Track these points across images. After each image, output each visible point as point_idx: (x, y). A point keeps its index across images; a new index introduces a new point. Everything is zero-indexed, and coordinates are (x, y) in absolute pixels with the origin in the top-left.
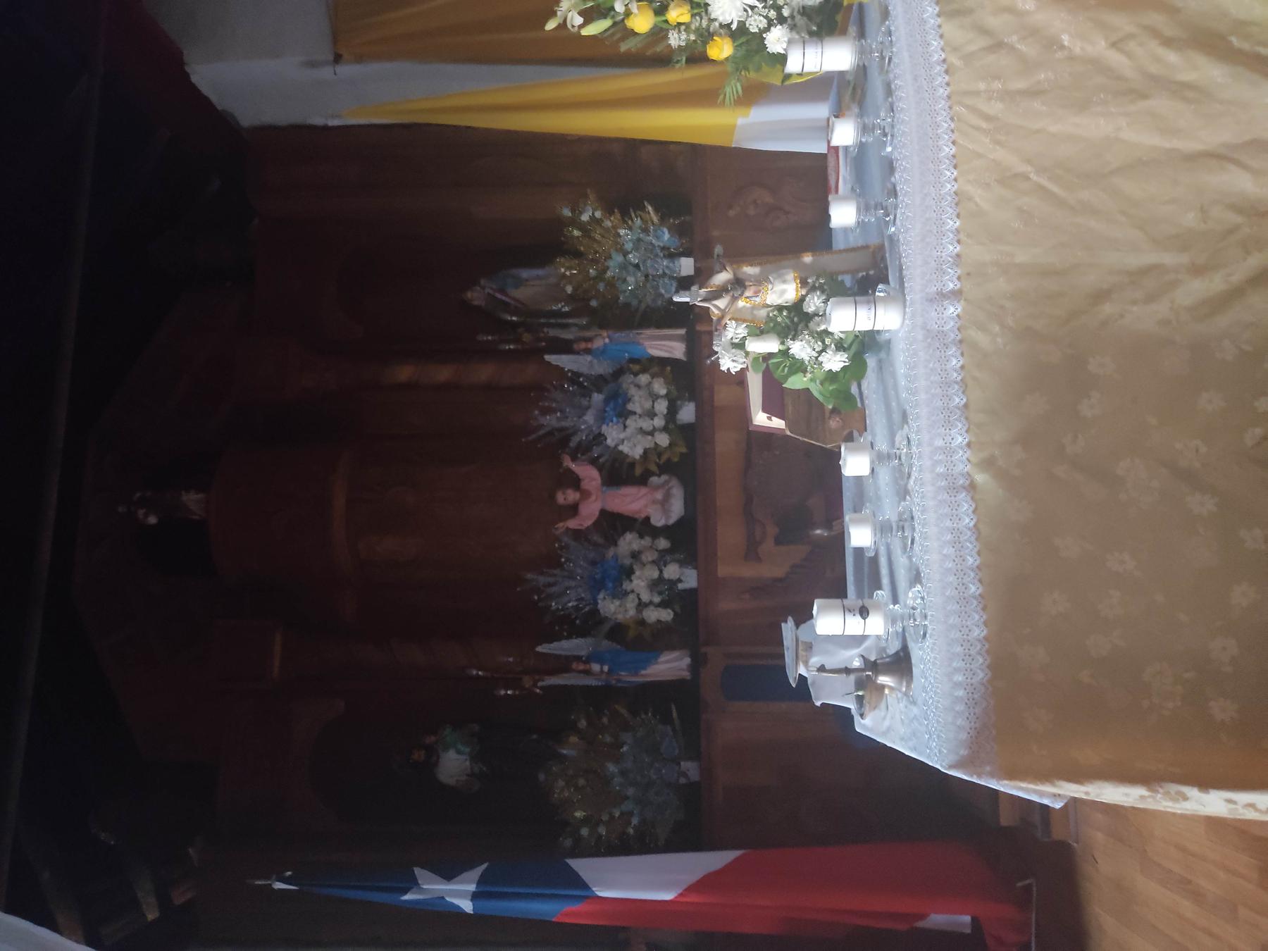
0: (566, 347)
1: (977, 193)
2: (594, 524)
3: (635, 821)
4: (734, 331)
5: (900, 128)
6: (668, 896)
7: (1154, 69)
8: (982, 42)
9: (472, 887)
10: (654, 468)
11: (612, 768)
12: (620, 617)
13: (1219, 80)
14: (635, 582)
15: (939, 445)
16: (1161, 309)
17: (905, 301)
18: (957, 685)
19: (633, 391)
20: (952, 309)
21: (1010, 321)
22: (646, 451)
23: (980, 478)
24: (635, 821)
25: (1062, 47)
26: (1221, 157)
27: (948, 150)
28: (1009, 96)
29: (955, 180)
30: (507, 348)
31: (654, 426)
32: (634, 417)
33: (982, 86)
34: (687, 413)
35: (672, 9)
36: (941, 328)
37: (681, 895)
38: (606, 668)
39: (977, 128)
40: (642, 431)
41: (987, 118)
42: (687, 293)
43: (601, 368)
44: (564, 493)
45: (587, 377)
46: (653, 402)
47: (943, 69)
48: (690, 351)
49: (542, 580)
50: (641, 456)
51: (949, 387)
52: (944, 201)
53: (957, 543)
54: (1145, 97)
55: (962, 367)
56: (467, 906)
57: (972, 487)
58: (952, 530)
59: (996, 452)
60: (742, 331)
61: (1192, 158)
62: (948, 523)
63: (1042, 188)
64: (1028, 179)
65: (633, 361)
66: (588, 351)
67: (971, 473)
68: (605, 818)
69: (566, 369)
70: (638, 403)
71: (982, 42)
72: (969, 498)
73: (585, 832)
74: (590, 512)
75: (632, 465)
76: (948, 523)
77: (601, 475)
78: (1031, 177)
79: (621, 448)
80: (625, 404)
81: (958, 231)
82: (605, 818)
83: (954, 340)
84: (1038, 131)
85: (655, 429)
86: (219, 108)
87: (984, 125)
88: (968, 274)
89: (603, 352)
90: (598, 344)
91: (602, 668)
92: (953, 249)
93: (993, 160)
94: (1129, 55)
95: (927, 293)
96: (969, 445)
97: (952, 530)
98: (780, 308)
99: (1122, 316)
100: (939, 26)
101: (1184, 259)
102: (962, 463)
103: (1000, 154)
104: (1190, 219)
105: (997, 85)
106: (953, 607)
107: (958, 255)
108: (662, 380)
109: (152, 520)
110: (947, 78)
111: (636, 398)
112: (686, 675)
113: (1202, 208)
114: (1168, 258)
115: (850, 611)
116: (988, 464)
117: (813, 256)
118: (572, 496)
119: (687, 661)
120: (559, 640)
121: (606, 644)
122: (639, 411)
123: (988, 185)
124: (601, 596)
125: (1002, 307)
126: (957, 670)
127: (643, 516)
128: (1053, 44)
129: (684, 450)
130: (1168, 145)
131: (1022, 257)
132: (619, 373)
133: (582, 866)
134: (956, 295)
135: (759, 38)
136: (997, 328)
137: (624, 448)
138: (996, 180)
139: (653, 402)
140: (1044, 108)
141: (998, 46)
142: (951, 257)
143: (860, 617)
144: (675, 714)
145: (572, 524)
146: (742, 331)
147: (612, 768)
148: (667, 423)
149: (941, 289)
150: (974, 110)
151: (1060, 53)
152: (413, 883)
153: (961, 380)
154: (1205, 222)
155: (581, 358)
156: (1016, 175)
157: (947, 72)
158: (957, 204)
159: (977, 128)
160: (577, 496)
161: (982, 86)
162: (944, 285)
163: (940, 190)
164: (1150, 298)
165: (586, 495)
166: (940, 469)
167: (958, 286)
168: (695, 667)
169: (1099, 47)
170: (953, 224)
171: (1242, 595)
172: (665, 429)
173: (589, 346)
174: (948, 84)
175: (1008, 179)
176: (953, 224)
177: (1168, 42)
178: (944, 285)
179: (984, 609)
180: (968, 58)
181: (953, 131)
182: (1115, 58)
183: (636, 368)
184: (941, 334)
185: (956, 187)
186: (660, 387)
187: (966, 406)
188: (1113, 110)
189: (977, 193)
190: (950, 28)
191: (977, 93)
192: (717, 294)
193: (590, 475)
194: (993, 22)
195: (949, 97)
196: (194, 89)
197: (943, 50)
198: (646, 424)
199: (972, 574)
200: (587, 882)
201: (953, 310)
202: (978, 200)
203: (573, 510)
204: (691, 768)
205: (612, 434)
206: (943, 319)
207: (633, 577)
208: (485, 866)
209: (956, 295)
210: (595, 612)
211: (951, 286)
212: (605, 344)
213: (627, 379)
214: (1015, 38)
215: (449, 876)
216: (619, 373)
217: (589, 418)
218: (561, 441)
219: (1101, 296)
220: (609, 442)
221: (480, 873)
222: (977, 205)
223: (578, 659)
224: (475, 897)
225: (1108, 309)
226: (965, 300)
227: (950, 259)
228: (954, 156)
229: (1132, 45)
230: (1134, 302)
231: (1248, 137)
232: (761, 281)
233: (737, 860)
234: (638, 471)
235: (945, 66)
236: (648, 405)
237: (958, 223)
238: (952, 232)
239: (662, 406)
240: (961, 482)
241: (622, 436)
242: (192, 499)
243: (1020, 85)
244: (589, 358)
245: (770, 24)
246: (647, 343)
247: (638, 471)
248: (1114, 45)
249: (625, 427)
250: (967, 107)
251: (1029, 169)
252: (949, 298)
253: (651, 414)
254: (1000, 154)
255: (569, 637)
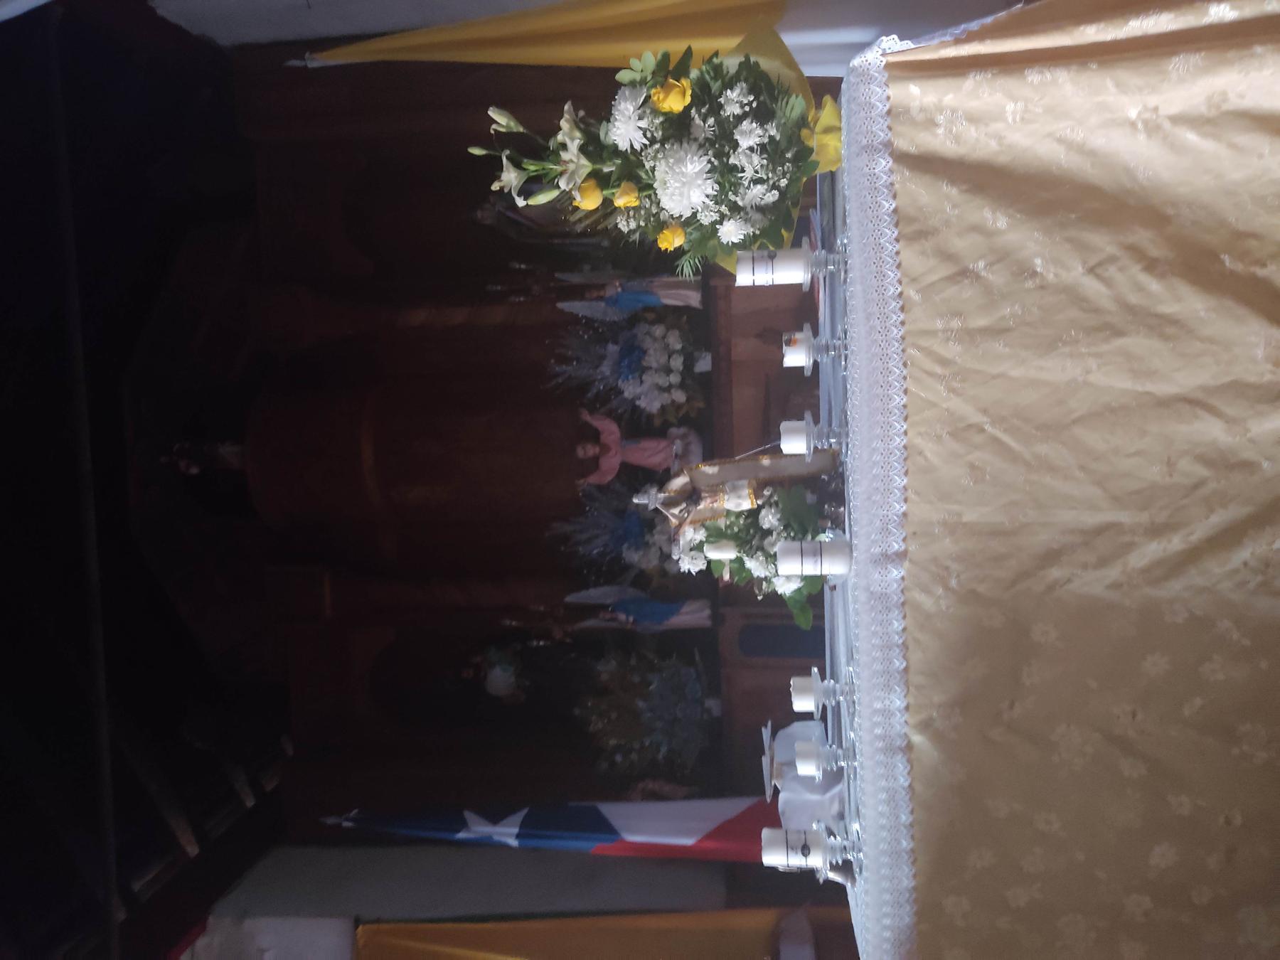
0: (577, 292)
1: (929, 448)
2: (618, 475)
3: (664, 750)
4: (691, 535)
5: (852, 347)
6: (688, 841)
7: (1133, 299)
8: (945, 270)
9: (516, 830)
10: (673, 420)
11: (641, 704)
12: (644, 566)
13: (1202, 314)
14: (656, 537)
15: (878, 707)
16: (1113, 573)
17: (851, 556)
18: (885, 928)
19: (648, 343)
20: (895, 572)
21: (953, 583)
22: (663, 408)
23: (917, 739)
24: (664, 750)
25: (1034, 274)
26: (1194, 403)
27: (899, 400)
28: (969, 336)
29: (906, 433)
30: (517, 300)
31: (670, 382)
32: (650, 372)
33: (939, 324)
34: (704, 364)
35: (618, 198)
36: (884, 590)
37: (700, 841)
38: (631, 619)
39: (930, 374)
40: (662, 389)
41: (943, 362)
42: (646, 496)
43: (614, 315)
44: (583, 448)
45: (603, 323)
46: (669, 357)
47: (899, 306)
48: (705, 300)
49: (567, 528)
50: (658, 410)
51: (890, 650)
52: (892, 455)
53: (892, 800)
54: (1119, 333)
55: (904, 630)
56: (514, 842)
57: (909, 747)
58: (888, 790)
59: (934, 714)
60: (701, 535)
61: (1165, 404)
62: (883, 783)
63: (996, 440)
64: (982, 430)
65: (648, 309)
66: (600, 298)
67: (908, 733)
68: (637, 746)
69: (580, 315)
70: (654, 358)
71: (945, 270)
72: (904, 760)
73: (618, 758)
74: (610, 464)
75: (650, 417)
76: (883, 783)
77: (620, 426)
78: (986, 428)
79: (638, 403)
80: (640, 359)
81: (905, 488)
82: (637, 746)
83: (897, 602)
84: (995, 377)
85: (671, 386)
86: (225, 37)
87: (938, 370)
88: (914, 533)
89: (613, 302)
90: (610, 292)
91: (627, 619)
92: (900, 508)
93: (947, 410)
94: (1107, 282)
95: (872, 555)
96: (907, 708)
97: (888, 790)
98: (739, 514)
99: (1069, 581)
100: (897, 253)
101: (1144, 518)
102: (900, 724)
103: (956, 404)
104: (1154, 473)
105: (956, 324)
106: (885, 860)
107: (905, 514)
108: (677, 333)
109: (194, 470)
110: (902, 317)
111: (651, 352)
112: (708, 623)
113: (1169, 459)
114: (1124, 517)
115: (792, 849)
116: (925, 726)
117: (771, 459)
118: (591, 450)
119: (707, 612)
120: (587, 587)
121: (631, 592)
122: (654, 365)
123: (939, 438)
124: (625, 546)
125: (947, 568)
126: (886, 915)
127: (665, 466)
128: (1025, 271)
129: (701, 405)
130: (1140, 388)
131: (970, 516)
132: (634, 320)
133: (612, 811)
134: (901, 556)
135: (712, 230)
136: (940, 591)
137: (642, 403)
138: (948, 433)
139: (669, 357)
140: (1007, 350)
141: (964, 274)
142: (897, 516)
143: (801, 855)
144: (697, 658)
145: (593, 479)
146: (701, 535)
147: (641, 704)
148: (683, 379)
149: (887, 550)
150: (928, 352)
151: (1031, 282)
152: (463, 825)
153: (903, 643)
154: (1171, 475)
155: (594, 303)
156: (970, 426)
157: (902, 309)
158: (905, 459)
159: (930, 374)
160: (597, 450)
161: (939, 324)
162: (889, 546)
163: (888, 444)
164: (1103, 562)
165: (605, 449)
166: (878, 731)
167: (903, 548)
168: (716, 617)
169: (1075, 273)
170: (901, 481)
171: (1162, 856)
172: (682, 386)
173: (602, 293)
174: (903, 323)
175: (961, 431)
176: (901, 481)
177: (1151, 266)
178: (889, 546)
179: (914, 863)
180: (926, 291)
181: (905, 378)
182: (1093, 287)
183: (651, 316)
184: (883, 597)
185: (905, 441)
186: (675, 342)
187: (906, 670)
188: (1083, 350)
189: (929, 448)
190: (910, 257)
191: (932, 333)
192: (670, 503)
193: (610, 430)
194: (960, 244)
195: (903, 338)
196: (163, 20)
197: (900, 282)
198: (662, 380)
199: (905, 831)
200: (616, 828)
201: (896, 573)
202: (929, 455)
203: (594, 463)
204: (713, 705)
205: (630, 390)
206: (886, 582)
207: (654, 532)
208: (525, 811)
209: (901, 556)
210: (618, 558)
211: (896, 547)
212: (617, 293)
213: (642, 329)
214: (981, 264)
215: (495, 819)
216: (634, 320)
217: (606, 369)
218: (577, 394)
219: (1051, 557)
220: (626, 394)
221: (522, 818)
222: (926, 458)
223: (604, 607)
224: (518, 836)
225: (1055, 573)
226: (911, 561)
227: (895, 518)
228: (905, 406)
229: (1112, 271)
230: (1085, 566)
231: (1227, 379)
232: (716, 489)
233: (750, 809)
234: (657, 422)
235: (901, 303)
236: (663, 359)
237: (905, 481)
238: (898, 489)
239: (677, 363)
240: (898, 743)
241: (639, 390)
242: (228, 451)
243: (981, 322)
244: (603, 304)
245: (723, 217)
246: (661, 293)
247: (657, 422)
248: (1091, 271)
249: (642, 382)
250: (920, 348)
251: (985, 419)
252: (893, 561)
253: (668, 371)
254: (956, 404)
255: (596, 585)
